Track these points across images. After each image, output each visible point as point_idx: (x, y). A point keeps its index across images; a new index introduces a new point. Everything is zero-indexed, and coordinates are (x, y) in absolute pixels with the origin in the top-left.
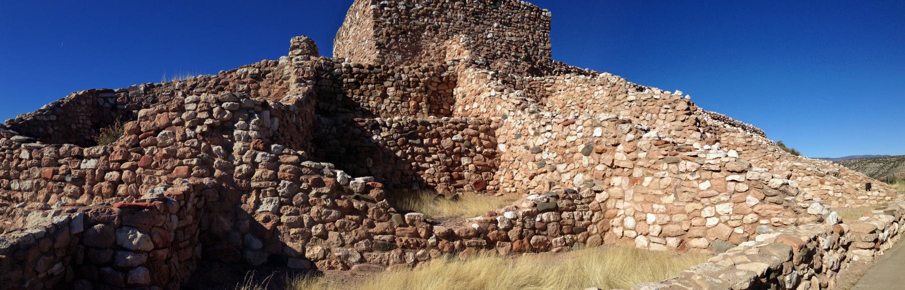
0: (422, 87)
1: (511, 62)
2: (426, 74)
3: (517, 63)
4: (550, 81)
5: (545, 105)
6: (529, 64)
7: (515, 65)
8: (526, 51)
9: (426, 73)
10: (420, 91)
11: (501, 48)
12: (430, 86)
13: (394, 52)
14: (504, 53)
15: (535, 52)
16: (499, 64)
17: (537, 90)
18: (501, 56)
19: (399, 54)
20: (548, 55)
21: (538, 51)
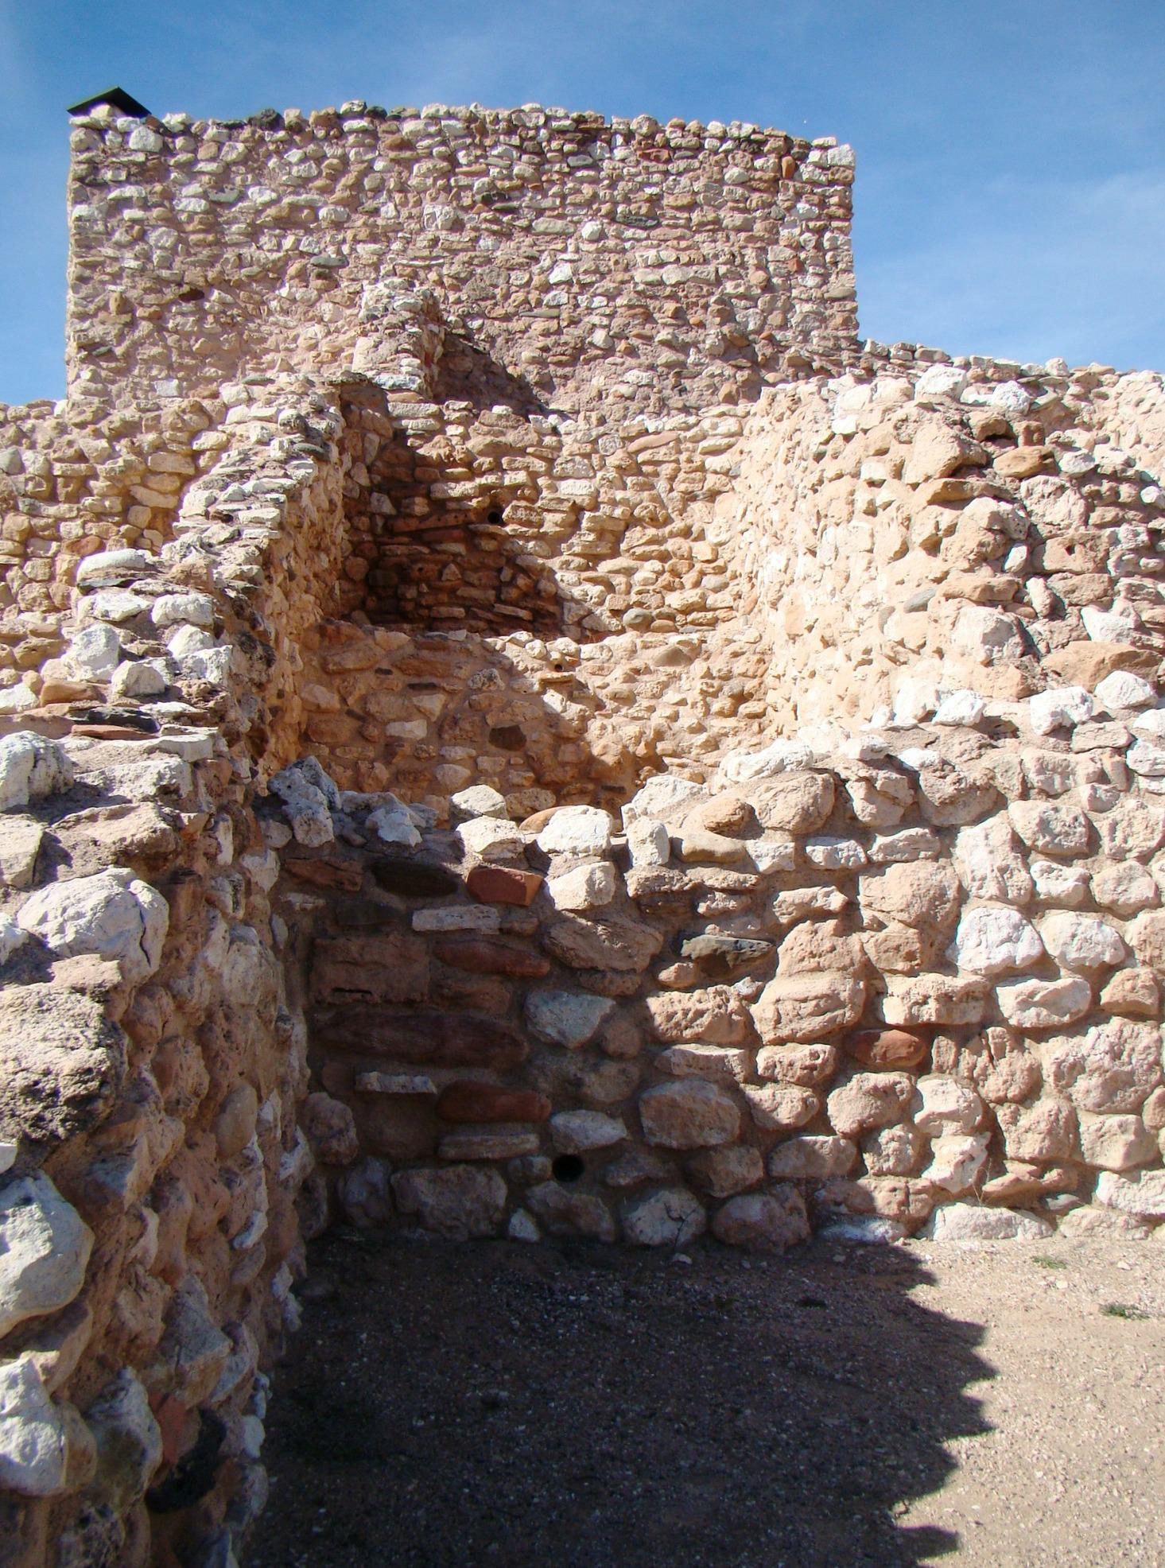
0: (104, 496)
1: (652, 367)
2: (122, 446)
3: (679, 370)
4: (722, 428)
5: (701, 536)
6: (740, 368)
7: (671, 380)
8: (727, 315)
9: (124, 442)
10: (100, 516)
11: (611, 316)
12: (140, 493)
13: (150, 369)
14: (621, 336)
15: (775, 318)
16: (598, 381)
17: (666, 470)
18: (609, 351)
19: (168, 378)
20: (838, 320)
21: (789, 308)
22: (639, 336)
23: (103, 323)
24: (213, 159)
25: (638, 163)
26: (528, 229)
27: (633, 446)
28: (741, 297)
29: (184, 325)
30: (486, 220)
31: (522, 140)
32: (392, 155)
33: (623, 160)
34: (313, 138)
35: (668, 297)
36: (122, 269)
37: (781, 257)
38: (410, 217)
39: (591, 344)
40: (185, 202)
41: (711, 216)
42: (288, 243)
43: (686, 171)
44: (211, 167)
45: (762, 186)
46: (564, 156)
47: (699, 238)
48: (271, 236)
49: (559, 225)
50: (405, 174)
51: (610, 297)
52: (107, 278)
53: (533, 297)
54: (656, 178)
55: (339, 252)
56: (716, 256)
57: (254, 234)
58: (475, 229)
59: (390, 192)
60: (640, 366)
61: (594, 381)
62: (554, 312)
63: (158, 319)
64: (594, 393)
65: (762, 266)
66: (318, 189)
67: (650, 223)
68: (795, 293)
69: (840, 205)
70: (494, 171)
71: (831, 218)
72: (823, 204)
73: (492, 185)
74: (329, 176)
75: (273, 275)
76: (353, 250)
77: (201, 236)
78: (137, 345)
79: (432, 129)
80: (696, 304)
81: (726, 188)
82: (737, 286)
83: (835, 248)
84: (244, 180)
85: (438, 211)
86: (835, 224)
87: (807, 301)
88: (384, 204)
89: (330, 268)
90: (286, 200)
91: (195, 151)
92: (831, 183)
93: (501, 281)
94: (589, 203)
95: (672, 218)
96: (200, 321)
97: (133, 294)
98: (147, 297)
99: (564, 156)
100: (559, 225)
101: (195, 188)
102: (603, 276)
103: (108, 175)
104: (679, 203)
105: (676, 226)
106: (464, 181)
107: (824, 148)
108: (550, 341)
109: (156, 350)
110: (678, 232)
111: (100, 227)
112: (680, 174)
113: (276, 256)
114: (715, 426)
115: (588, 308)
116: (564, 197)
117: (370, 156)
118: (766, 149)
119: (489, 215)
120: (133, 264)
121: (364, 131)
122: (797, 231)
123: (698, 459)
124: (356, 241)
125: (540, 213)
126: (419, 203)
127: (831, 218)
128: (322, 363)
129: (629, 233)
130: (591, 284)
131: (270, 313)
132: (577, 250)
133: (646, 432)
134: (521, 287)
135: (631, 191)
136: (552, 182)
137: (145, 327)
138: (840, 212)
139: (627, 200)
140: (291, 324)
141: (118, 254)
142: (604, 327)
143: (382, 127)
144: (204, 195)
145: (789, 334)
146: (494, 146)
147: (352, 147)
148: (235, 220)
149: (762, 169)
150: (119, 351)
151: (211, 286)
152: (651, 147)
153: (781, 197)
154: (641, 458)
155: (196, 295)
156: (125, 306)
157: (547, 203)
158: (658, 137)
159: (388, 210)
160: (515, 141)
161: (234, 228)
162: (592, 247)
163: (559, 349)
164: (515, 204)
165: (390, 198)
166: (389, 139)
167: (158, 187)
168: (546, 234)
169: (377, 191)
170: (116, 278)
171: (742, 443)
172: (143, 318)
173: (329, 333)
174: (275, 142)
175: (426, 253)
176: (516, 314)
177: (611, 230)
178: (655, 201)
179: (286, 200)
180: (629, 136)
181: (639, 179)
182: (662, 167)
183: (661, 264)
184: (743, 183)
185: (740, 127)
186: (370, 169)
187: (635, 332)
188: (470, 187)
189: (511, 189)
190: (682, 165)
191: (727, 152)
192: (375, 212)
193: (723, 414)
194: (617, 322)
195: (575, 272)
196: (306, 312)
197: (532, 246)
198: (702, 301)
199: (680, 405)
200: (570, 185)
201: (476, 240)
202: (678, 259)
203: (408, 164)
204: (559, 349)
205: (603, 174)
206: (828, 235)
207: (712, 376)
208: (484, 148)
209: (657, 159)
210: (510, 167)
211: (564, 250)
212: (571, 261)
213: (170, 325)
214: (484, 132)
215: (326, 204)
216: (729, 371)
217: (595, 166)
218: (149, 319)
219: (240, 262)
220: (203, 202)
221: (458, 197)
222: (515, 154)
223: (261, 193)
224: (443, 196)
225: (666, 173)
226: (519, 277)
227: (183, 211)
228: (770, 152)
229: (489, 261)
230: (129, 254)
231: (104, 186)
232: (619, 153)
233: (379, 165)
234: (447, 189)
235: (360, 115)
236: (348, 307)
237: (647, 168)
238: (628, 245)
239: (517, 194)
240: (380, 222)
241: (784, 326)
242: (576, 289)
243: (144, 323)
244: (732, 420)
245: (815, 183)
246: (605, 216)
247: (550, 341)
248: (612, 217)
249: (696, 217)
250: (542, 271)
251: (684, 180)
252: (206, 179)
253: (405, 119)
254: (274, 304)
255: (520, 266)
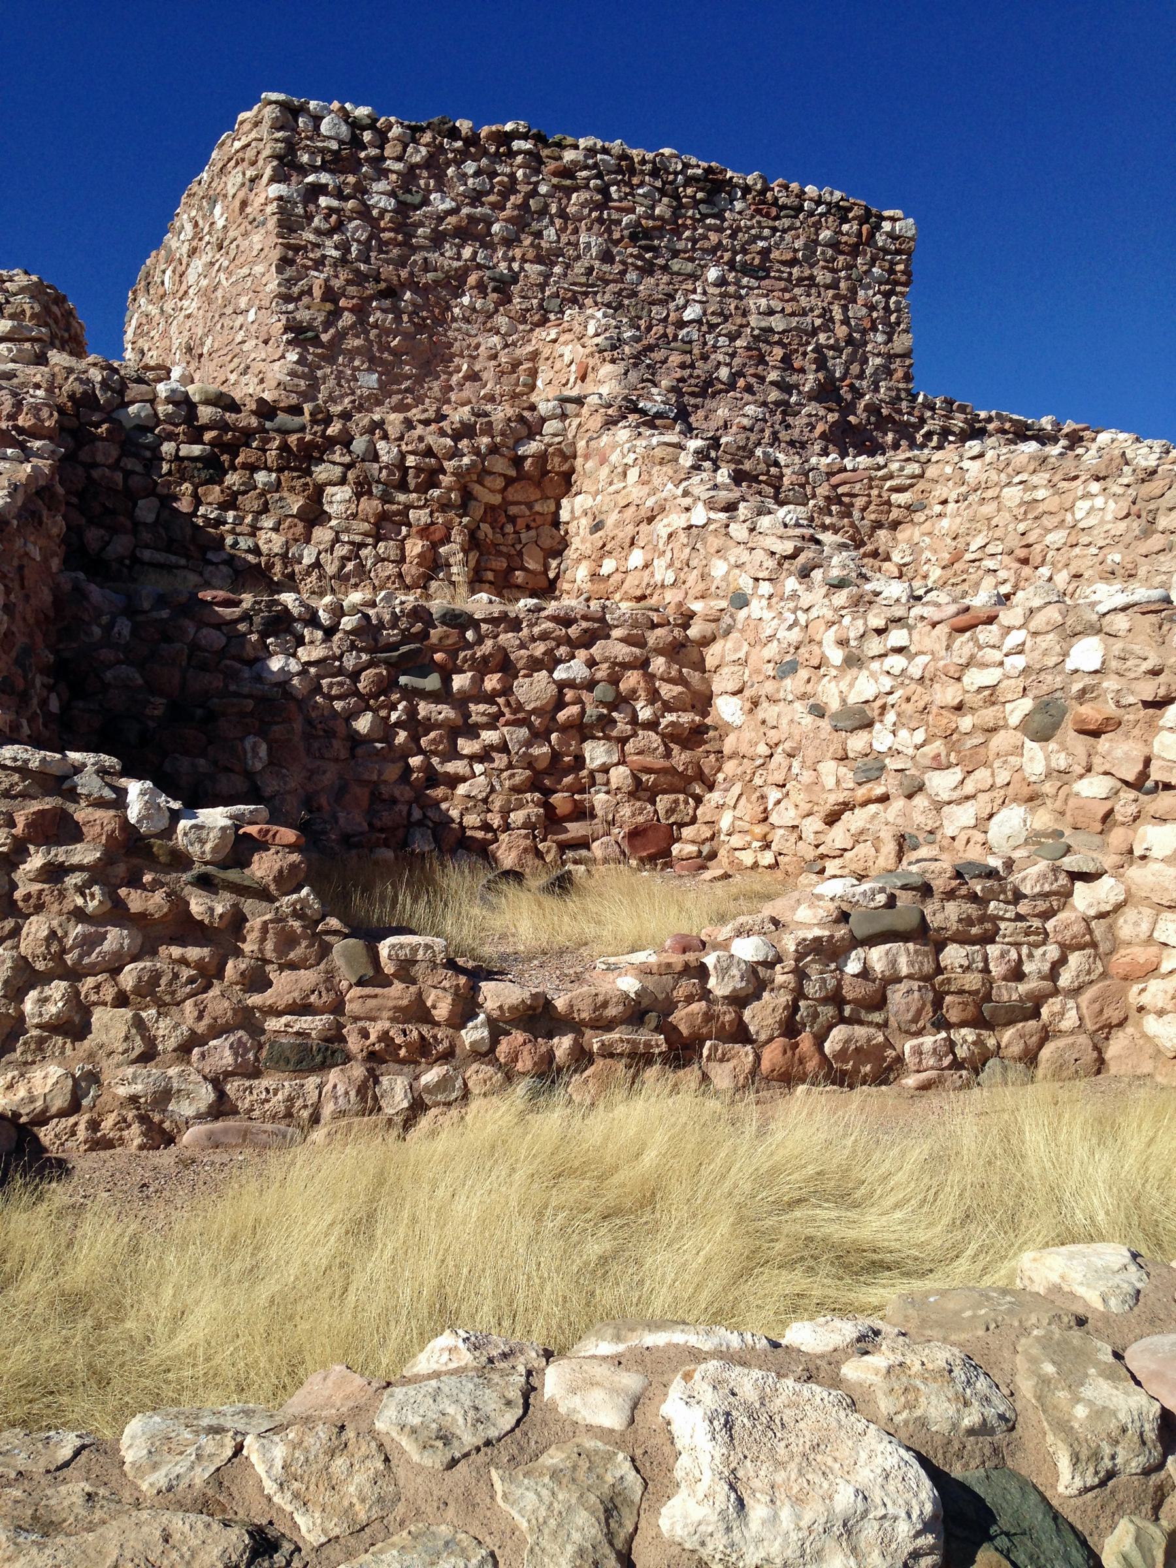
1: (764, 404)
6: (831, 410)
7: (779, 417)
8: (821, 363)
13: (352, 360)
14: (740, 374)
15: (855, 369)
16: (722, 412)
18: (731, 386)
20: (900, 374)
21: (865, 361)
22: (754, 375)
23: (308, 308)
24: (399, 159)
25: (753, 217)
26: (665, 268)
27: (835, 480)
28: (831, 347)
29: (384, 320)
30: (631, 255)
31: (664, 183)
32: (555, 180)
33: (740, 213)
34: (485, 153)
35: (776, 343)
36: (324, 257)
37: (859, 315)
38: (569, 243)
39: (717, 378)
40: (376, 198)
41: (807, 273)
42: (467, 252)
43: (790, 228)
44: (398, 166)
45: (846, 249)
46: (696, 203)
47: (798, 291)
48: (452, 244)
49: (689, 267)
50: (564, 201)
51: (733, 337)
52: (310, 263)
53: (670, 330)
54: (766, 232)
55: (510, 268)
56: (812, 310)
57: (437, 239)
58: (623, 263)
59: (551, 217)
60: (756, 402)
61: (720, 412)
62: (687, 347)
63: (361, 311)
64: (721, 423)
65: (846, 322)
66: (490, 204)
67: (761, 274)
68: (869, 347)
69: (903, 272)
70: (640, 210)
71: (897, 283)
72: (891, 271)
73: (638, 224)
74: (500, 193)
75: (455, 282)
76: (522, 269)
77: (392, 235)
78: (341, 336)
79: (590, 162)
80: (797, 351)
81: (819, 249)
82: (829, 338)
83: (898, 310)
84: (427, 185)
85: (590, 240)
86: (898, 289)
87: (879, 355)
88: (546, 227)
89: (503, 283)
90: (465, 211)
91: (382, 148)
92: (898, 252)
93: (645, 313)
94: (713, 250)
95: (779, 271)
96: (398, 319)
97: (337, 284)
98: (349, 288)
99: (696, 203)
100: (689, 267)
101: (382, 186)
102: (726, 320)
103: (305, 158)
104: (784, 258)
105: (780, 279)
106: (615, 216)
107: (893, 220)
108: (686, 373)
109: (357, 342)
110: (782, 284)
111: (300, 210)
112: (784, 231)
113: (456, 264)
114: (902, 469)
115: (714, 346)
116: (695, 241)
117: (534, 179)
118: (851, 215)
119: (635, 251)
120: (336, 254)
121: (527, 152)
122: (871, 292)
123: (885, 495)
124: (524, 260)
125: (675, 254)
126: (576, 231)
127: (897, 283)
128: (503, 373)
129: (745, 281)
130: (718, 325)
131: (454, 319)
132: (705, 293)
133: (844, 470)
134: (660, 321)
135: (747, 243)
136: (686, 227)
137: (347, 319)
138: (903, 278)
139: (744, 251)
140: (473, 332)
141: (319, 240)
142: (727, 365)
143: (545, 152)
144: (392, 194)
145: (865, 383)
146: (641, 184)
147: (519, 167)
148: (421, 224)
149: (847, 234)
150: (325, 338)
151: (403, 286)
152: (764, 205)
153: (859, 260)
154: (840, 490)
155: (391, 293)
156: (330, 295)
157: (680, 245)
158: (769, 194)
159: (550, 233)
160: (659, 184)
161: (420, 231)
162: (717, 291)
163: (693, 381)
164: (656, 242)
165: (552, 223)
166: (552, 165)
167: (351, 179)
168: (678, 274)
169: (544, 211)
170: (319, 264)
171: (921, 485)
172: (346, 309)
173: (506, 346)
174: (453, 151)
175: (583, 280)
176: (657, 345)
177: (731, 277)
178: (765, 253)
179: (465, 211)
180: (747, 189)
181: (753, 232)
182: (771, 223)
183: (771, 312)
184: (834, 245)
185: (832, 194)
186: (534, 193)
187: (752, 371)
188: (619, 222)
189: (653, 228)
190: (786, 222)
191: (822, 215)
192: (538, 235)
193: (908, 459)
194: (737, 361)
195: (705, 314)
196: (484, 323)
197: (668, 284)
198: (801, 349)
199: (788, 439)
200: (700, 231)
201: (623, 273)
202: (783, 310)
203: (569, 191)
204: (693, 381)
205: (726, 224)
206: (894, 299)
207: (810, 415)
208: (632, 187)
209: (767, 215)
210: (653, 208)
211: (694, 291)
212: (700, 302)
213: (371, 320)
214: (632, 171)
215: (498, 220)
216: (822, 412)
217: (720, 216)
218: (351, 310)
219: (427, 266)
220: (393, 201)
221: (609, 231)
222: (657, 196)
223: (443, 200)
224: (596, 226)
225: (774, 230)
226: (658, 312)
227: (374, 207)
228: (854, 218)
229: (634, 294)
230: (328, 243)
231: (303, 170)
232: (738, 205)
233: (543, 189)
234: (600, 220)
235: (525, 137)
236: (521, 323)
237: (759, 222)
238: (743, 292)
239: (657, 233)
240: (543, 244)
241: (861, 376)
242: (704, 328)
243: (346, 313)
244: (916, 465)
245: (886, 251)
246: (726, 264)
247: (686, 373)
248: (732, 265)
249: (796, 271)
250: (677, 309)
251: (788, 237)
252: (393, 177)
253: (565, 147)
254: (456, 311)
255: (660, 302)
